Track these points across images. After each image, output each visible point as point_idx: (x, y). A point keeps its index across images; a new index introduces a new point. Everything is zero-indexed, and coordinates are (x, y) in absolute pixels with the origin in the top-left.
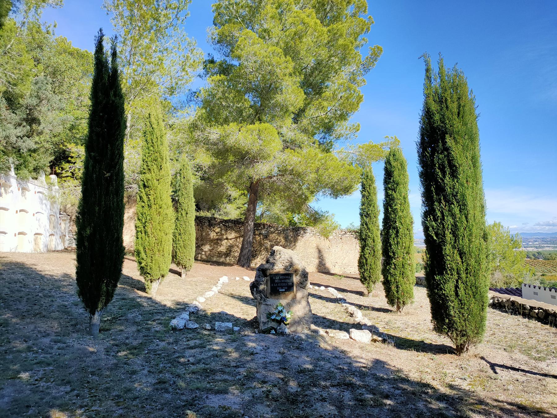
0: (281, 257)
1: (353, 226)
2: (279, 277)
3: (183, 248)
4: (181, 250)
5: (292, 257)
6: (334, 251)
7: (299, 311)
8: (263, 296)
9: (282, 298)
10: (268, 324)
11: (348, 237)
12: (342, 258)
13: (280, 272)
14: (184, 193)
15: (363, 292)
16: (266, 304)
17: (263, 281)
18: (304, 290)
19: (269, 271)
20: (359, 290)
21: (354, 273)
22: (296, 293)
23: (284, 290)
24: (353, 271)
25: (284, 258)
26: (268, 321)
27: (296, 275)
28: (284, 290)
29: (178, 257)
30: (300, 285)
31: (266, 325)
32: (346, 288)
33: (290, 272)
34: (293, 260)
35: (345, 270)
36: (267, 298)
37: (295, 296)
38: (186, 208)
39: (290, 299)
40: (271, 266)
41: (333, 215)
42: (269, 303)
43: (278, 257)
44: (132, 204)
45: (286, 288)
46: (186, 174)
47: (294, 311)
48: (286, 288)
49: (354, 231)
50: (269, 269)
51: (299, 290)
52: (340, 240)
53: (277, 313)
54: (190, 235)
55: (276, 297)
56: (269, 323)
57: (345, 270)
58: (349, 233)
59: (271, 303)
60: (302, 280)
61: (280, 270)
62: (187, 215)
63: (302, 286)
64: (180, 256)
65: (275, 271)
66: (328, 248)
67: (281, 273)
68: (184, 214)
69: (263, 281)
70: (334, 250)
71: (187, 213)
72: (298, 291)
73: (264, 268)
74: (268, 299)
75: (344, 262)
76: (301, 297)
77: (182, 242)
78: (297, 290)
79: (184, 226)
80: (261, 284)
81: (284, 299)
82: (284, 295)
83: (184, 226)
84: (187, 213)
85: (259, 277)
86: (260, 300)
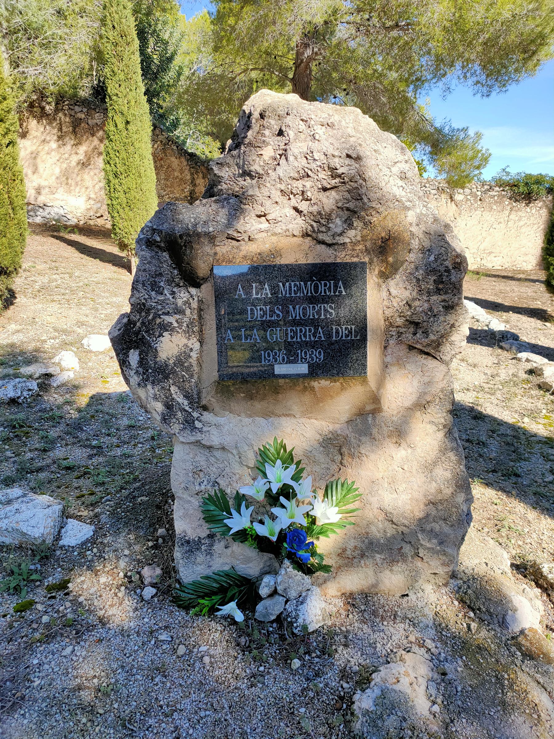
0: (284, 154)
1: (508, 173)
2: (274, 290)
3: (127, 209)
4: (121, 211)
5: (366, 151)
6: (463, 225)
7: (393, 481)
8: (180, 399)
9: (296, 409)
10: (209, 553)
11: (494, 196)
12: (480, 238)
13: (276, 253)
14: (116, 69)
15: (545, 311)
16: (198, 443)
17: (179, 311)
18: (431, 363)
19: (207, 249)
20: (537, 305)
21: (500, 268)
22: (381, 383)
23: (303, 368)
24: (499, 263)
25: (309, 156)
26: (211, 536)
27: (384, 276)
28: (303, 368)
29: (118, 230)
30: (408, 337)
31: (200, 557)
32: (500, 301)
33: (343, 257)
34: (371, 173)
35: (483, 262)
36: (205, 408)
37: (376, 399)
38: (125, 109)
39: (345, 417)
40: (222, 216)
41: (478, 136)
42: (214, 439)
43: (268, 152)
44: (82, 136)
45: (319, 356)
46: (116, 16)
47: (361, 485)
48: (319, 356)
49: (509, 185)
50: (212, 238)
51: (400, 363)
52: (479, 203)
53: (261, 497)
54: (140, 176)
55: (258, 405)
56: (219, 547)
57: (483, 262)
58: (497, 189)
59: (228, 441)
60: (421, 305)
61: (284, 242)
62: (129, 127)
63: (421, 341)
64: (121, 226)
65: (251, 249)
66: (453, 219)
67: (287, 260)
68: (121, 126)
69: (179, 311)
70: (464, 223)
71: (128, 123)
72: (393, 369)
73: (178, 229)
74: (207, 416)
75: (482, 247)
76: (408, 403)
77: (122, 195)
78: (385, 366)
79: (123, 154)
80: (166, 327)
81: (308, 412)
82: (307, 398)
83: (123, 154)
84: (128, 123)
85: (155, 287)
86: (165, 419)
